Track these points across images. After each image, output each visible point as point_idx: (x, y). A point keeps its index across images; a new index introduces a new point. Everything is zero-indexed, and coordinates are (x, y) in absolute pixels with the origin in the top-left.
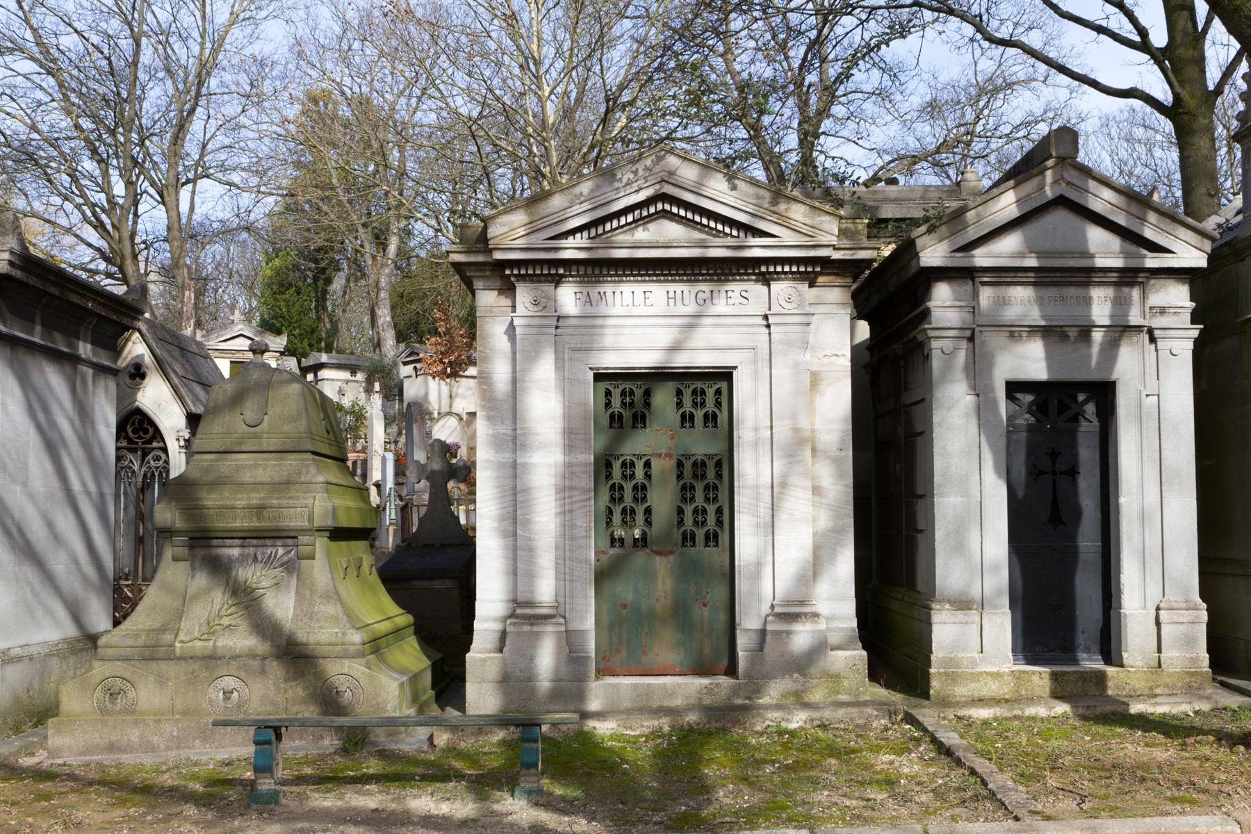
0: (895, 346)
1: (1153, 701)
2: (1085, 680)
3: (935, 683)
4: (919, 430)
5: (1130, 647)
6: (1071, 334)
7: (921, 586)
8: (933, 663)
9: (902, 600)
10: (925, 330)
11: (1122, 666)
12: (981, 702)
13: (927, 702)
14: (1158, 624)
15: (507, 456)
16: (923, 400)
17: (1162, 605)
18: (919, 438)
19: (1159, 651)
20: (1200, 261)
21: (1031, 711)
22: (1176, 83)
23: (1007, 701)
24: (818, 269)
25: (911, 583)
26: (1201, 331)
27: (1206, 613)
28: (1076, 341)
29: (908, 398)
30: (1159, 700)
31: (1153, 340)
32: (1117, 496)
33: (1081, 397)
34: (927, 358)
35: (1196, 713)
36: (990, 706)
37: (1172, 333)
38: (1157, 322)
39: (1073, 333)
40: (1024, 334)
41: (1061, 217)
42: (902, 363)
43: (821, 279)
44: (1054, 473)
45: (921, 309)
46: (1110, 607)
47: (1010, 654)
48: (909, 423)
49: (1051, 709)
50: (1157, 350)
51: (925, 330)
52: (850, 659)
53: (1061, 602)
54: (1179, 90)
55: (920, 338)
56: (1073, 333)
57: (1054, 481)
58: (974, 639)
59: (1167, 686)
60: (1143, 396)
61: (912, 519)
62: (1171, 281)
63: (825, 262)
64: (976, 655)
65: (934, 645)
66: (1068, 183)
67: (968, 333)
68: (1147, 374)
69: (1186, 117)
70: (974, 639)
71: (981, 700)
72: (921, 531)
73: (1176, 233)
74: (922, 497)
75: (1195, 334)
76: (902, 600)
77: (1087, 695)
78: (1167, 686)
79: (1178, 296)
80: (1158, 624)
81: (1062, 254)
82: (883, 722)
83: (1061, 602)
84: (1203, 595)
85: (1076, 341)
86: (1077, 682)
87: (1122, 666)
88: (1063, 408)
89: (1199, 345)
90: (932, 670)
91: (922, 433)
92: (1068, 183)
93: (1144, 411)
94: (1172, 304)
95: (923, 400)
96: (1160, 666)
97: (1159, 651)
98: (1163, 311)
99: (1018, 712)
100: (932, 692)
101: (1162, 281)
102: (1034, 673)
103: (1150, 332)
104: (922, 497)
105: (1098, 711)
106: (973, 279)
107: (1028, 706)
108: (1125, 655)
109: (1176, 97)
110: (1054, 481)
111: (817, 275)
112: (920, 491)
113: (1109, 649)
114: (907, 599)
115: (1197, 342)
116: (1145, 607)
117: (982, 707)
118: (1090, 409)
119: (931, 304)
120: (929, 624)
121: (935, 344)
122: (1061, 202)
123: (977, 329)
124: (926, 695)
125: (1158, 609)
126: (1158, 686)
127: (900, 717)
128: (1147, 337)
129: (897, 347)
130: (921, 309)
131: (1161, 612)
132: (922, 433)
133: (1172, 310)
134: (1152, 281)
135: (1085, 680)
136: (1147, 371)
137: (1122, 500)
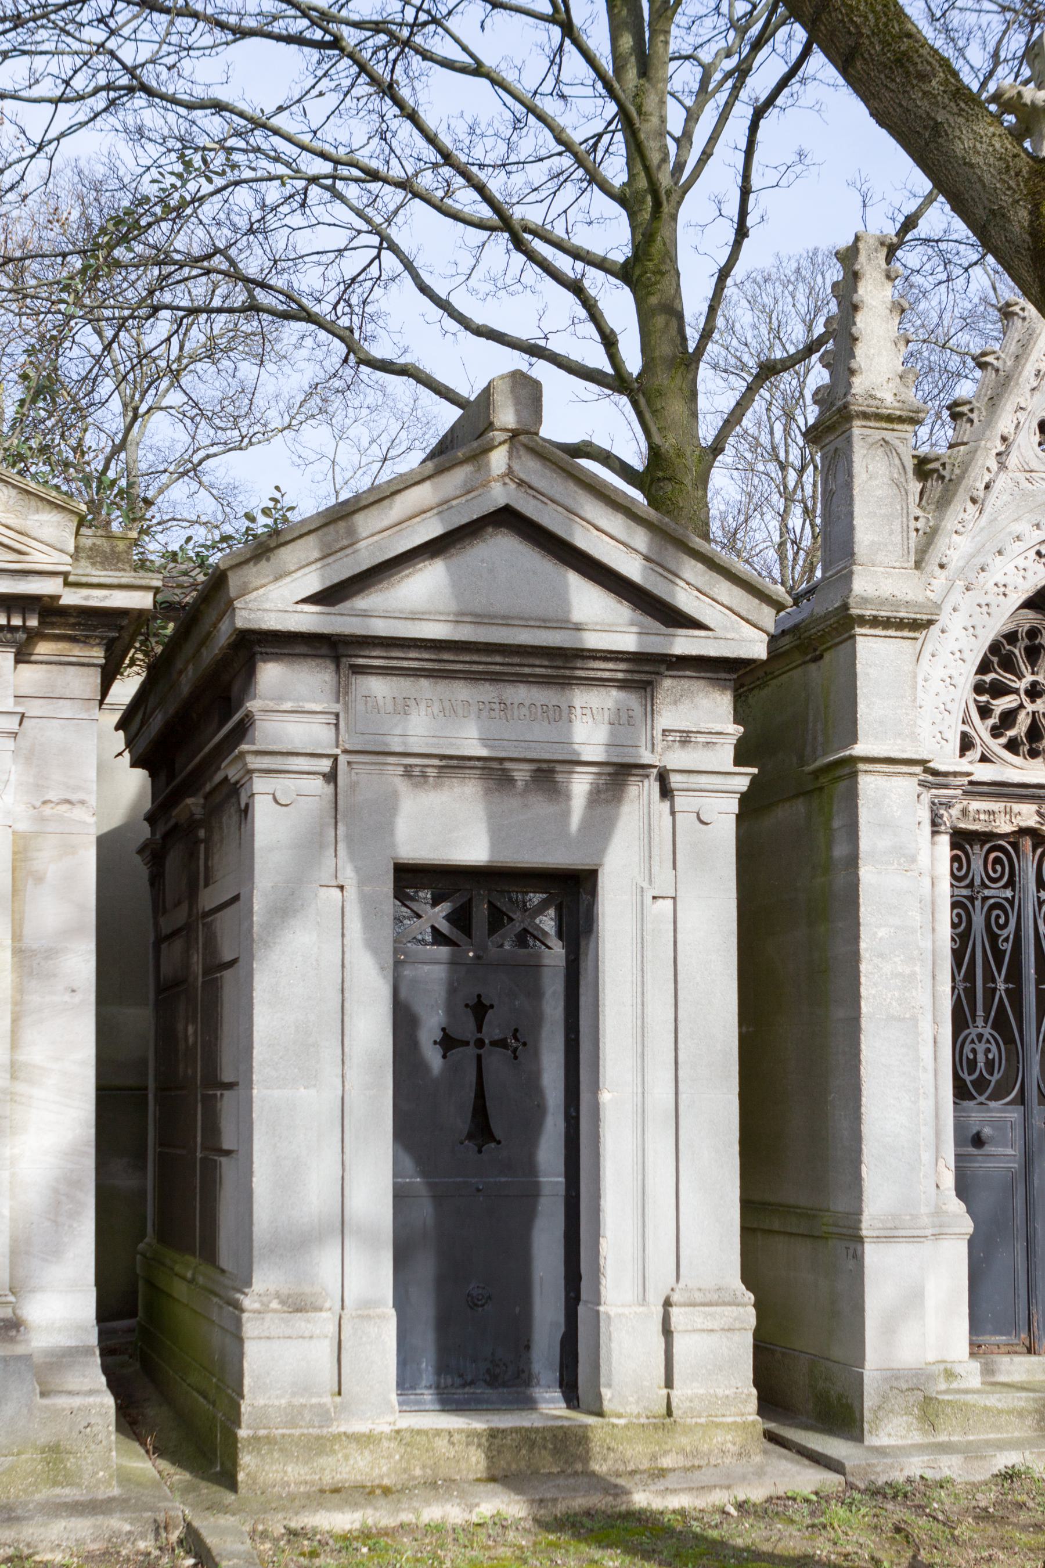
0: (189, 801)
1: (661, 1485)
2: (533, 1444)
3: (247, 1460)
4: (227, 957)
5: (616, 1379)
6: (517, 775)
7: (225, 1260)
8: (244, 1419)
9: (192, 1281)
10: (242, 754)
11: (600, 1414)
12: (336, 1494)
13: (230, 1498)
14: (667, 1332)
15: (22, 1057)
16: (236, 898)
17: (675, 1298)
18: (227, 974)
19: (669, 1383)
20: (757, 648)
21: (433, 1513)
22: (654, 429)
23: (387, 1491)
24: (33, 622)
25: (209, 1253)
26: (755, 780)
27: (752, 1311)
28: (526, 790)
29: (208, 899)
30: (671, 1481)
31: (666, 792)
32: (595, 1087)
33: (536, 898)
34: (246, 812)
35: (740, 1506)
36: (355, 1506)
37: (704, 780)
38: (676, 759)
39: (521, 774)
40: (431, 772)
41: (503, 548)
42: (202, 833)
43: (43, 648)
44: (480, 1043)
45: (236, 718)
46: (577, 1299)
47: (393, 1397)
48: (211, 945)
49: (471, 1508)
50: (673, 813)
51: (242, 754)
52: (91, 1396)
53: (494, 1303)
54: (657, 439)
55: (233, 773)
56: (521, 774)
57: (479, 1058)
58: (323, 1324)
59: (682, 1451)
60: (648, 899)
61: (213, 1129)
62: (701, 683)
63: (48, 609)
64: (327, 1400)
65: (247, 1381)
66: (521, 483)
67: (325, 765)
68: (656, 859)
69: (669, 487)
70: (323, 1324)
71: (336, 1491)
72: (228, 1153)
73: (715, 592)
74: (230, 1086)
75: (742, 783)
76: (192, 1281)
77: (536, 1472)
78: (682, 1451)
79: (707, 716)
80: (667, 1332)
81: (506, 621)
82: (142, 1545)
83: (494, 1303)
84: (749, 1277)
85: (526, 790)
86: (519, 1448)
87: (600, 1414)
88: (497, 920)
89: (750, 806)
90: (243, 1433)
91: (233, 962)
92: (521, 483)
93: (648, 926)
94: (704, 726)
95: (236, 898)
96: (669, 1413)
97: (669, 1383)
98: (685, 738)
99: (406, 1517)
100: (241, 1476)
101: (685, 683)
102: (438, 1433)
103: (663, 777)
104: (230, 1086)
105: (560, 1509)
106: (337, 660)
107: (427, 1503)
108: (606, 1393)
109: (655, 454)
110: (479, 1058)
111: (34, 636)
112: (227, 1076)
113: (575, 1380)
114: (201, 1280)
115: (746, 800)
116: (644, 1301)
117: (339, 1508)
118: (548, 922)
119: (253, 705)
120: (240, 1340)
121: (260, 785)
122: (507, 518)
123: (343, 759)
124: (232, 1485)
125: (667, 1303)
126: (666, 1453)
127: (174, 1536)
128: (656, 787)
129: (193, 804)
130: (236, 718)
131: (674, 1311)
132: (233, 962)
133: (701, 739)
134: (667, 683)
135: (533, 1444)
136: (655, 851)
137: (605, 1097)
